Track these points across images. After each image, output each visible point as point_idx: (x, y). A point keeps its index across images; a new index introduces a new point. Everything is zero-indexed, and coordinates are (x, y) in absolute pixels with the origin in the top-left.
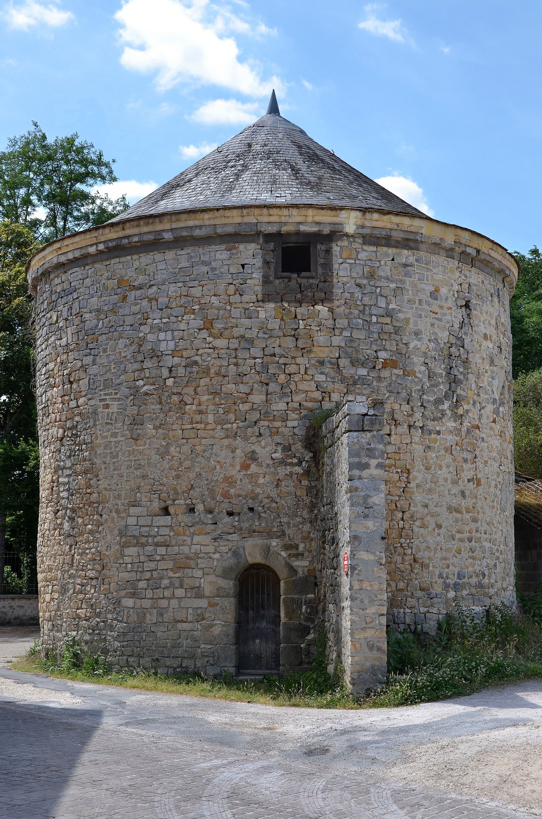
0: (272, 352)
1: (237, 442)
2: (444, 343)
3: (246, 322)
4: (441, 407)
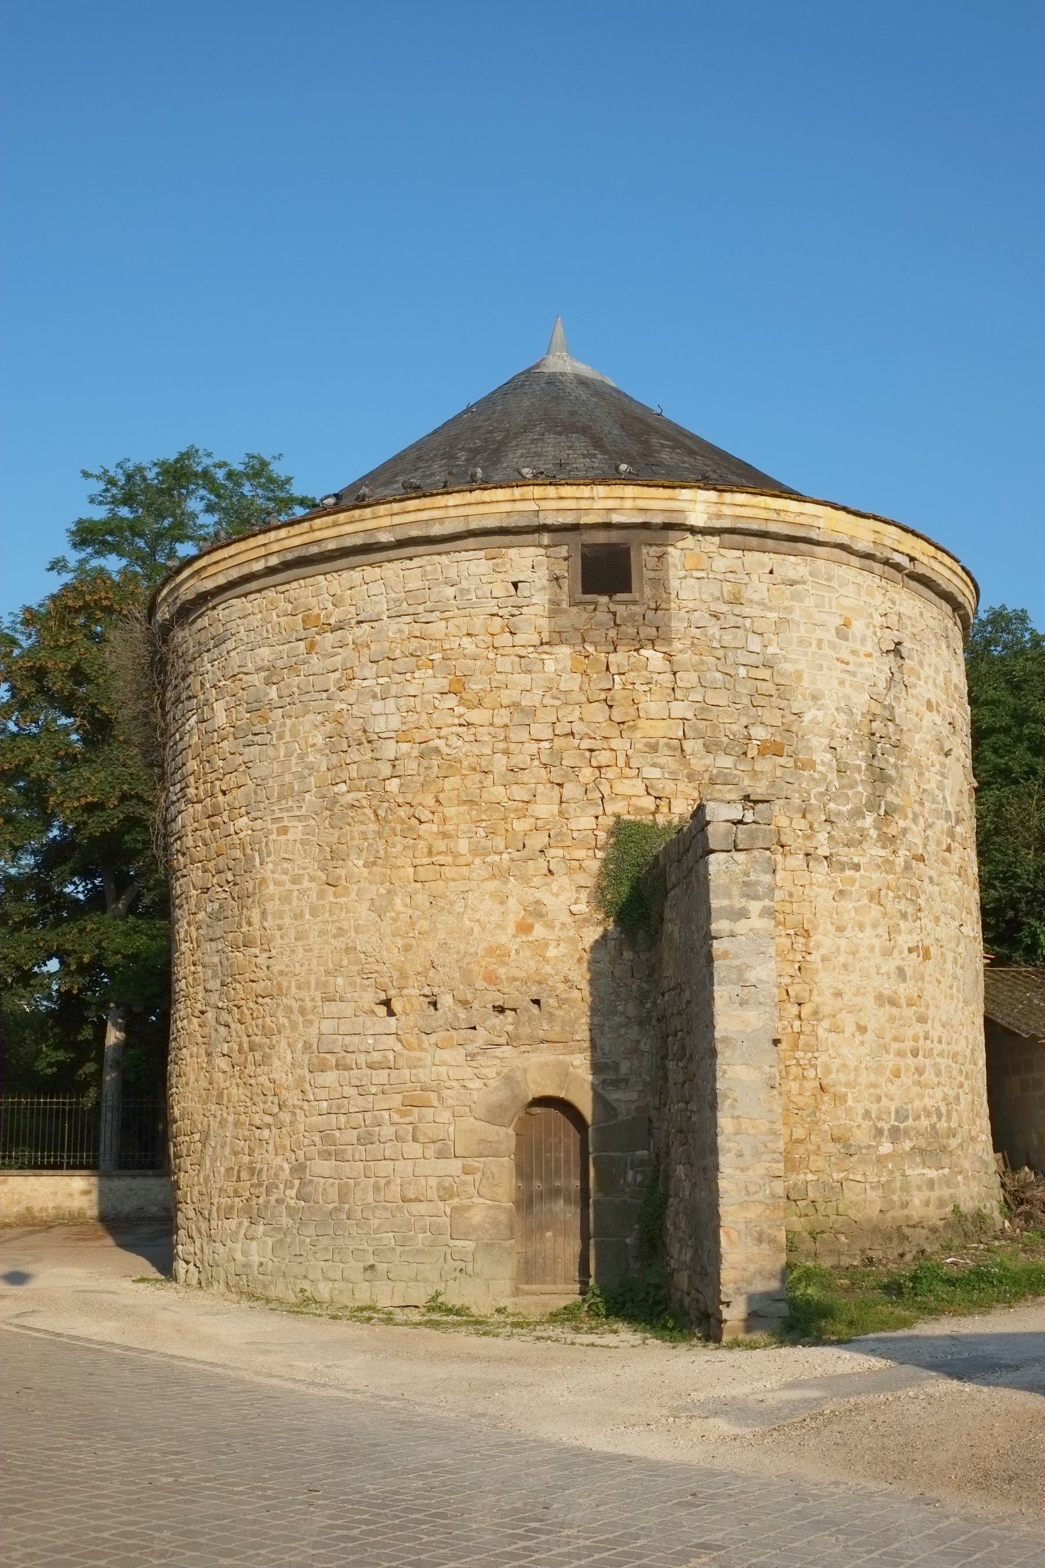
0: (568, 730)
1: (510, 886)
2: (863, 714)
3: (525, 680)
4: (859, 823)
